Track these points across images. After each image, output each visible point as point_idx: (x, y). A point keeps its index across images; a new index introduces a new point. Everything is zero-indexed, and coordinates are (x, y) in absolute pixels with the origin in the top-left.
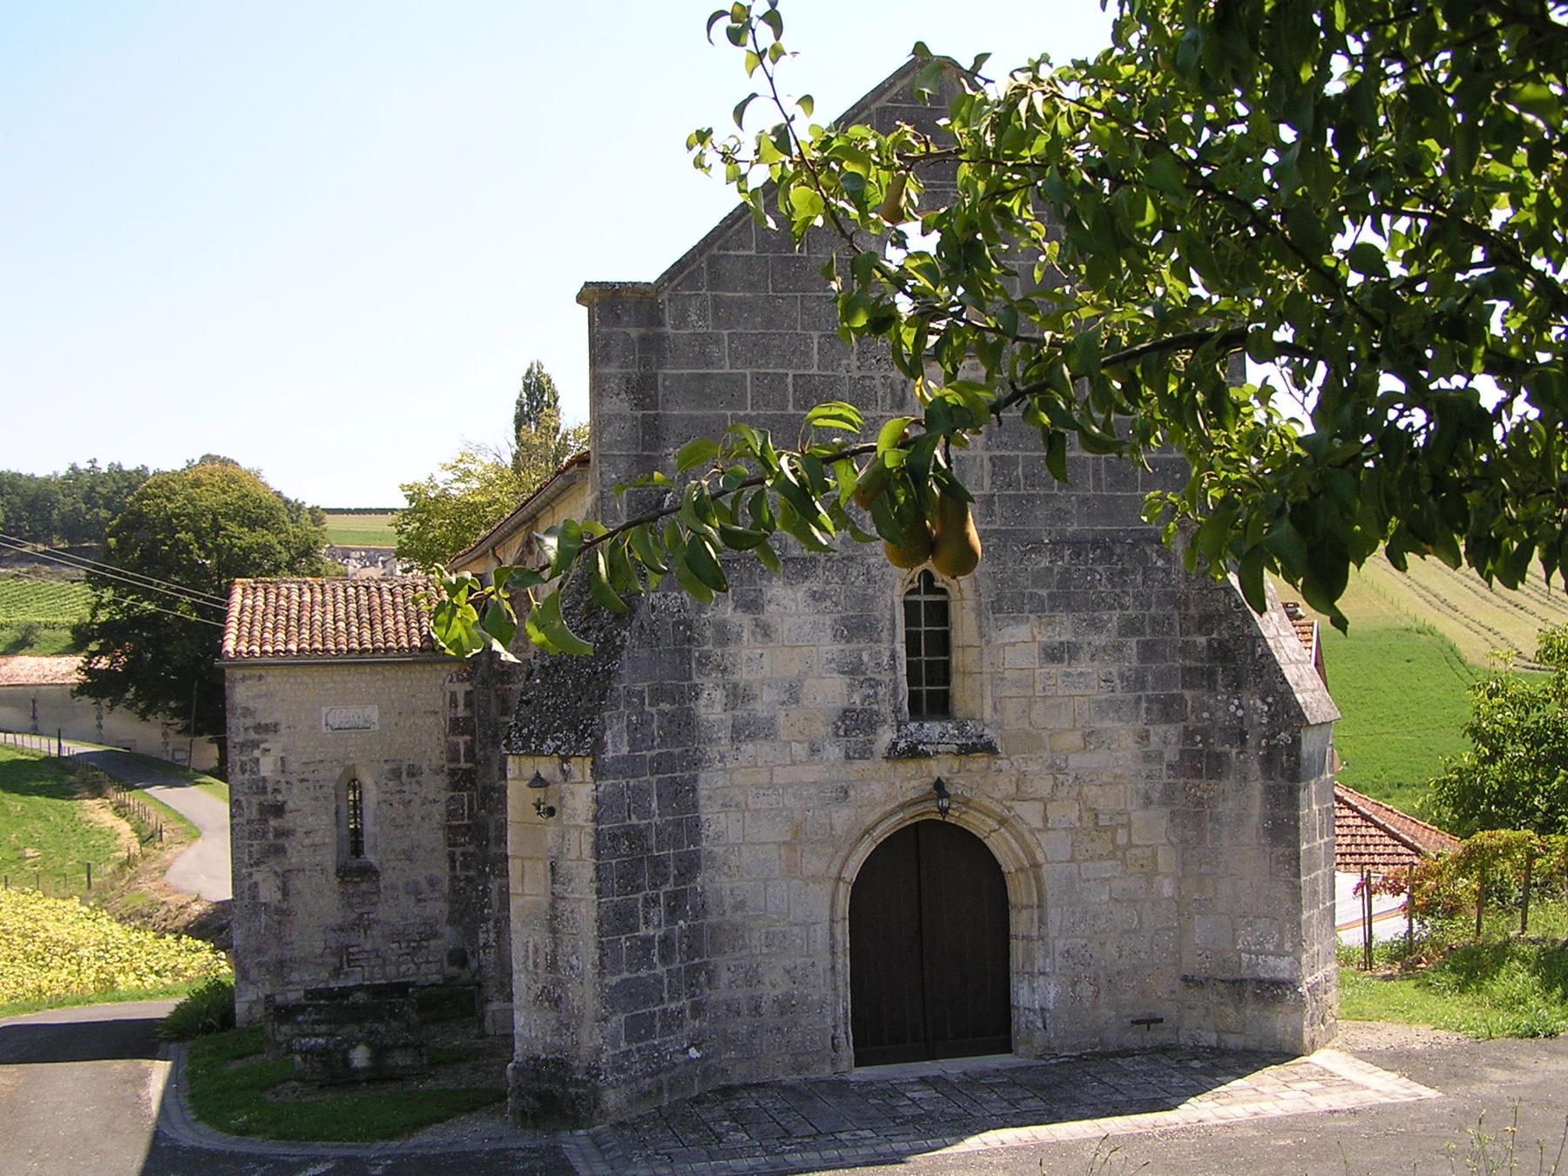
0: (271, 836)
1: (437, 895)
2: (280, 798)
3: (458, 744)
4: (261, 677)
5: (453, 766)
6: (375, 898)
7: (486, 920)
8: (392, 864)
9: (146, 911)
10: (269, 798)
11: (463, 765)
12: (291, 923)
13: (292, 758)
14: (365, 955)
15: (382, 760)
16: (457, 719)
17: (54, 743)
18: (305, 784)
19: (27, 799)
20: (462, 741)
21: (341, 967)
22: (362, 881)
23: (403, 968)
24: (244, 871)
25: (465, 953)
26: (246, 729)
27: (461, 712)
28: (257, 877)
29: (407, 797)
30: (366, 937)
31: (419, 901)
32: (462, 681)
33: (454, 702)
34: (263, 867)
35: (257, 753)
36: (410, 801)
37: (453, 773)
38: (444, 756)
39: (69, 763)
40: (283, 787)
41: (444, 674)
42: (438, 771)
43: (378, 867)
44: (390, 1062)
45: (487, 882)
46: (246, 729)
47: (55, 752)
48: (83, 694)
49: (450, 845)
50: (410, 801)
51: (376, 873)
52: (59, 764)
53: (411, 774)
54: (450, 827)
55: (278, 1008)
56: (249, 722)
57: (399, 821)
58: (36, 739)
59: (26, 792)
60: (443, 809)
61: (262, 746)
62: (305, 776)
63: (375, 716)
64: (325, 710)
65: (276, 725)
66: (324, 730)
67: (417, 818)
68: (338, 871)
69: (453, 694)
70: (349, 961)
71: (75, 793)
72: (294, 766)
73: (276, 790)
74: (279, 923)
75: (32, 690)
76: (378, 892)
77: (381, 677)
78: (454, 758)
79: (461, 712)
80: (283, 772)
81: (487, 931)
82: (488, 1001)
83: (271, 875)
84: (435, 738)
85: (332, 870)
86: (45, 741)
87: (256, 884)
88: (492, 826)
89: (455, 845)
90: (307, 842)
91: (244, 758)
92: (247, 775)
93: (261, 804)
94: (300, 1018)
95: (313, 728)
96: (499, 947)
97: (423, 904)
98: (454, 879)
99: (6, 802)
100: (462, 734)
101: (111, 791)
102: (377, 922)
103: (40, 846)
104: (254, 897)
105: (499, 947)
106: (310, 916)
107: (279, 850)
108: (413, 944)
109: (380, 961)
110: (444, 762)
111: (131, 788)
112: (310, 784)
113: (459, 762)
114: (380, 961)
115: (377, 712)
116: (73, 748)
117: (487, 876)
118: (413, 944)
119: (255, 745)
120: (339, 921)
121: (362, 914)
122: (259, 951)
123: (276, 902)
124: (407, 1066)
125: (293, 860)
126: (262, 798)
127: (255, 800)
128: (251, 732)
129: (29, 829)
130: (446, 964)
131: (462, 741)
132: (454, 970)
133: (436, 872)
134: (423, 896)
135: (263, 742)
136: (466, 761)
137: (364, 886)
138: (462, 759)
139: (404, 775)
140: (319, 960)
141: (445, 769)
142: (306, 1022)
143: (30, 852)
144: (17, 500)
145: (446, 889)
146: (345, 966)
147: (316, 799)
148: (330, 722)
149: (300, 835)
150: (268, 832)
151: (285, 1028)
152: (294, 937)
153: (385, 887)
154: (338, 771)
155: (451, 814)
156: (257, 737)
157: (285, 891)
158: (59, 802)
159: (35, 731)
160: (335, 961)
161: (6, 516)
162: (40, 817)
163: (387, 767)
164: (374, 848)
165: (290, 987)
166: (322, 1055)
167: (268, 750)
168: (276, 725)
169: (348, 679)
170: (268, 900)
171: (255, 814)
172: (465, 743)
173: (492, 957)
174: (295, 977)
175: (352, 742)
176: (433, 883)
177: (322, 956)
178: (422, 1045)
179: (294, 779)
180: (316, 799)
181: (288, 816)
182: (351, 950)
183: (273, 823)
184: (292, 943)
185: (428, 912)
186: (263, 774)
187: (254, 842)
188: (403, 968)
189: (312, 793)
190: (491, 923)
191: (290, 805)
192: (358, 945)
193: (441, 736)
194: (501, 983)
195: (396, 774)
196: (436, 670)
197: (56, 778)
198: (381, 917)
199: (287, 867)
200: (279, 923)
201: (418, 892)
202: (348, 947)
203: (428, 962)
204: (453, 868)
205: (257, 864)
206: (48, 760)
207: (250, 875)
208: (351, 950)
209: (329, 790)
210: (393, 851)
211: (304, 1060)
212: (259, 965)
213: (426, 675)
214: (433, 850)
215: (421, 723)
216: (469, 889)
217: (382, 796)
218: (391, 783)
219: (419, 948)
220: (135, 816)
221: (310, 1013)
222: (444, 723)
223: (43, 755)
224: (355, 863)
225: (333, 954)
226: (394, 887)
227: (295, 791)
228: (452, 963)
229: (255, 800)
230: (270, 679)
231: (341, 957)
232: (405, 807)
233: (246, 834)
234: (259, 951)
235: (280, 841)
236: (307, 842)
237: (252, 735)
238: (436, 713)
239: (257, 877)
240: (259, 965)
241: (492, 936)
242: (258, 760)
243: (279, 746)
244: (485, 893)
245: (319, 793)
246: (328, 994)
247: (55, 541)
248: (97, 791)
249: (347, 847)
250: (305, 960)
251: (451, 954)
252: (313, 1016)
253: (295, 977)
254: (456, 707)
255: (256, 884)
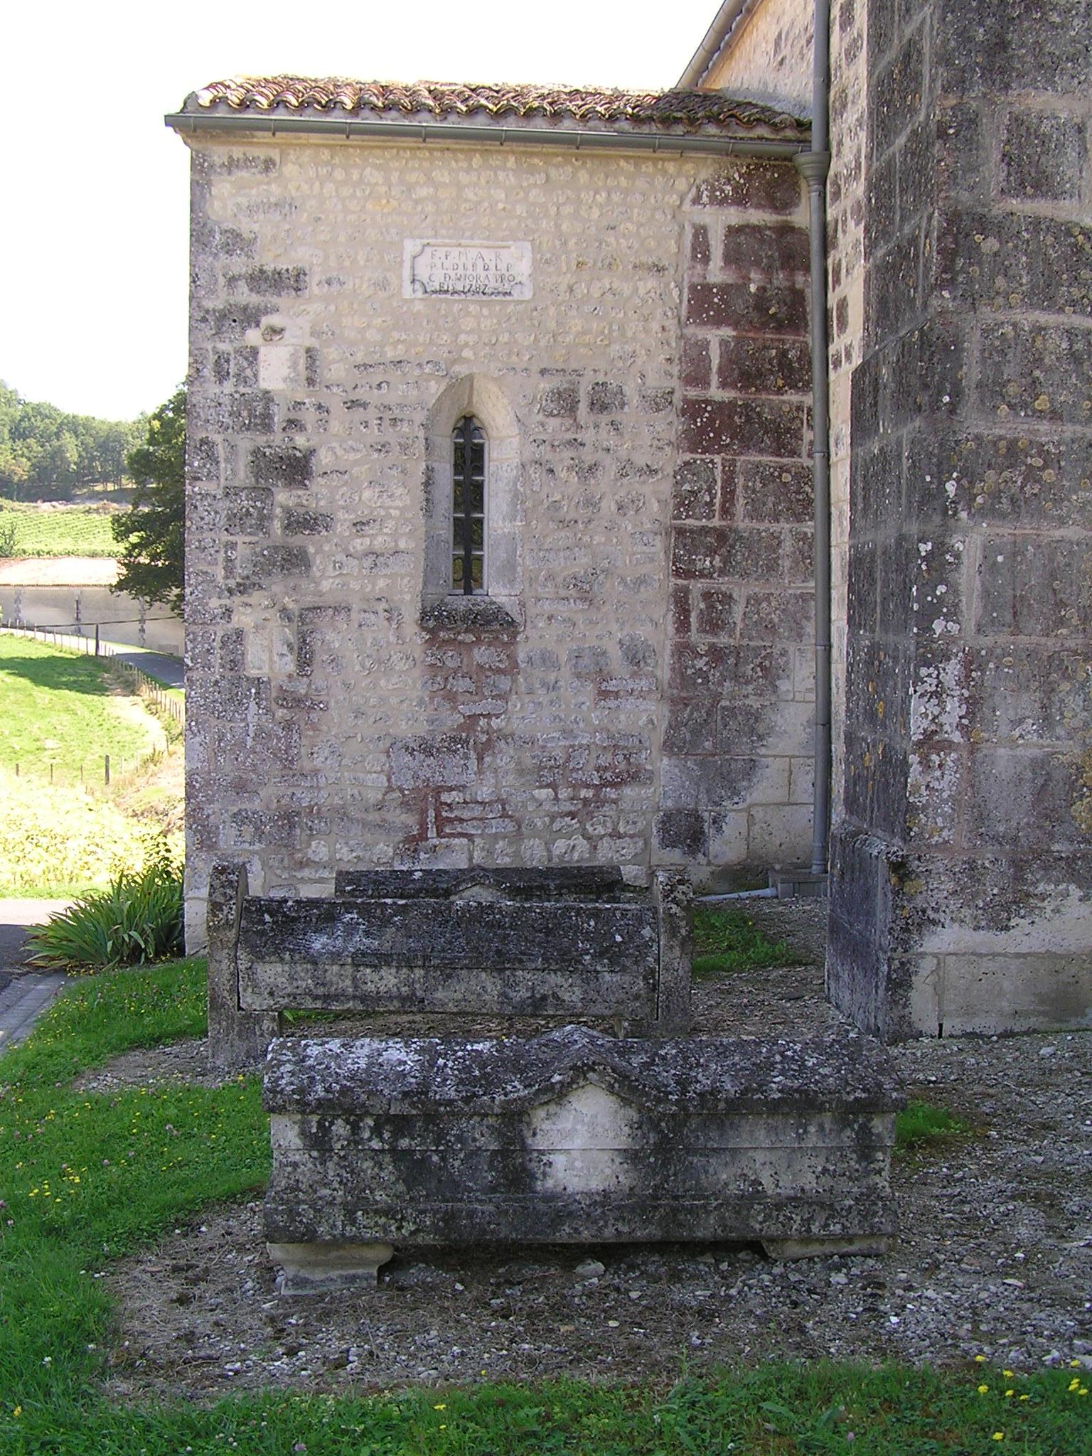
0: (277, 526)
1: (644, 684)
2: (300, 441)
3: (705, 345)
4: (269, 164)
5: (693, 393)
6: (504, 683)
7: (933, 656)
8: (547, 607)
9: (161, 808)
10: (278, 440)
11: (716, 393)
12: (314, 727)
13: (332, 353)
14: (478, 811)
15: (535, 368)
16: (707, 288)
17: (92, 643)
18: (359, 414)
19: (56, 692)
20: (716, 337)
21: (423, 836)
22: (479, 641)
23: (560, 846)
24: (214, 603)
25: (699, 818)
26: (232, 281)
27: (717, 273)
28: (243, 619)
29: (588, 456)
30: (480, 772)
31: (604, 694)
32: (723, 202)
33: (701, 251)
34: (256, 597)
35: (253, 336)
36: (593, 468)
37: (692, 409)
38: (675, 370)
39: (105, 661)
40: (309, 417)
41: (681, 184)
42: (659, 402)
43: (518, 619)
44: (723, 1175)
45: (946, 530)
46: (232, 281)
47: (92, 652)
48: (121, 590)
49: (677, 574)
50: (593, 468)
51: (511, 625)
52: (95, 663)
53: (599, 406)
54: (681, 532)
55: (254, 909)
56: (239, 264)
57: (567, 510)
58: (75, 639)
59: (56, 686)
60: (667, 488)
61: (265, 321)
62: (361, 394)
63: (523, 268)
64: (410, 247)
65: (300, 275)
66: (407, 291)
67: (608, 506)
68: (425, 615)
69: (701, 233)
70: (440, 822)
71: (107, 689)
72: (335, 369)
73: (293, 424)
74: (288, 726)
75: (77, 591)
76: (512, 669)
77: (539, 179)
78: (697, 378)
79: (717, 273)
80: (311, 382)
81: (938, 694)
82: (924, 921)
83: (273, 614)
84: (655, 326)
85: (411, 614)
86: (83, 640)
87: (240, 634)
88: (973, 346)
89: (689, 574)
90: (359, 544)
91: (224, 347)
92: (229, 386)
93: (256, 452)
94: (319, 943)
95: (383, 285)
96: (973, 748)
97: (612, 703)
98: (683, 650)
99: (34, 693)
100: (718, 322)
101: (144, 688)
102: (506, 737)
103: (63, 739)
104: (235, 664)
105: (973, 748)
106: (359, 714)
107: (294, 561)
108: (584, 793)
109: (510, 827)
110: (675, 383)
111: (166, 687)
112: (371, 414)
113: (706, 384)
114: (510, 827)
115: (528, 255)
116: (110, 648)
117: (947, 512)
118: (584, 793)
119: (250, 317)
120: (422, 729)
121: (474, 718)
122: (240, 787)
123: (281, 679)
124: (797, 1200)
125: (326, 585)
126: (261, 440)
127: (245, 443)
128: (242, 287)
129: (54, 721)
130: (655, 842)
131: (716, 337)
132: (675, 856)
133: (644, 632)
134: (612, 686)
135: (266, 311)
136: (723, 385)
137: (482, 655)
138: (715, 379)
139: (583, 408)
140: (373, 817)
141: (677, 399)
142: (336, 957)
143: (49, 744)
144: (90, 440)
145: (665, 674)
146: (432, 833)
147: (383, 448)
148: (423, 274)
149: (342, 528)
150: (270, 518)
151: (272, 972)
152: (318, 762)
153: (530, 660)
154: (435, 389)
155: (684, 502)
156: (254, 299)
157: (305, 659)
158: (90, 697)
159: (78, 633)
160: (411, 820)
161: (80, 456)
162: (67, 710)
163: (545, 385)
164: (510, 566)
165: (306, 873)
166: (401, 1125)
167: (276, 331)
168: (300, 275)
169: (464, 178)
170: (264, 673)
171: (244, 476)
172: (723, 343)
173: (947, 782)
174: (319, 850)
175: (469, 324)
176: (636, 657)
177: (380, 807)
178: (871, 1106)
179: (335, 402)
180: (383, 448)
181: (318, 485)
182: (445, 797)
183: (283, 497)
184: (316, 772)
185: (623, 722)
186: (264, 385)
187: (239, 539)
188: (560, 846)
189: (374, 435)
190: (952, 670)
191: (324, 459)
192: (461, 788)
193: (671, 324)
194: (971, 865)
195: (566, 402)
196: (664, 172)
197: (90, 675)
198: (516, 725)
199: (309, 601)
200: (288, 726)
201: (601, 675)
202: (439, 790)
203: (616, 835)
204: (683, 625)
205: (242, 589)
206: (85, 658)
207: (228, 612)
208: (445, 797)
209: (412, 430)
210: (551, 577)
211: (318, 1142)
212: (240, 818)
213: (641, 183)
214: (641, 581)
215: (626, 289)
216: (714, 675)
217: (531, 451)
218: (553, 423)
219: (600, 802)
220: (166, 715)
221: (351, 929)
222: (678, 297)
223: (80, 654)
224: (461, 603)
225: (405, 805)
226: (548, 660)
227: (335, 426)
228: (669, 841)
229: (245, 443)
230: (290, 169)
231: (424, 812)
232: (583, 479)
233: (222, 521)
234: (240, 787)
235: (297, 540)
236: (359, 544)
237: (244, 296)
238: (660, 270)
239: (243, 619)
240: (240, 818)
241: (954, 709)
242: (255, 352)
243: (305, 323)
244: (940, 562)
245: (390, 435)
246: (398, 883)
247: (124, 481)
248: (130, 689)
249: (446, 568)
250: (342, 814)
251: (668, 820)
252: (360, 941)
253: (319, 850)
254: (706, 259)
255: (240, 634)
